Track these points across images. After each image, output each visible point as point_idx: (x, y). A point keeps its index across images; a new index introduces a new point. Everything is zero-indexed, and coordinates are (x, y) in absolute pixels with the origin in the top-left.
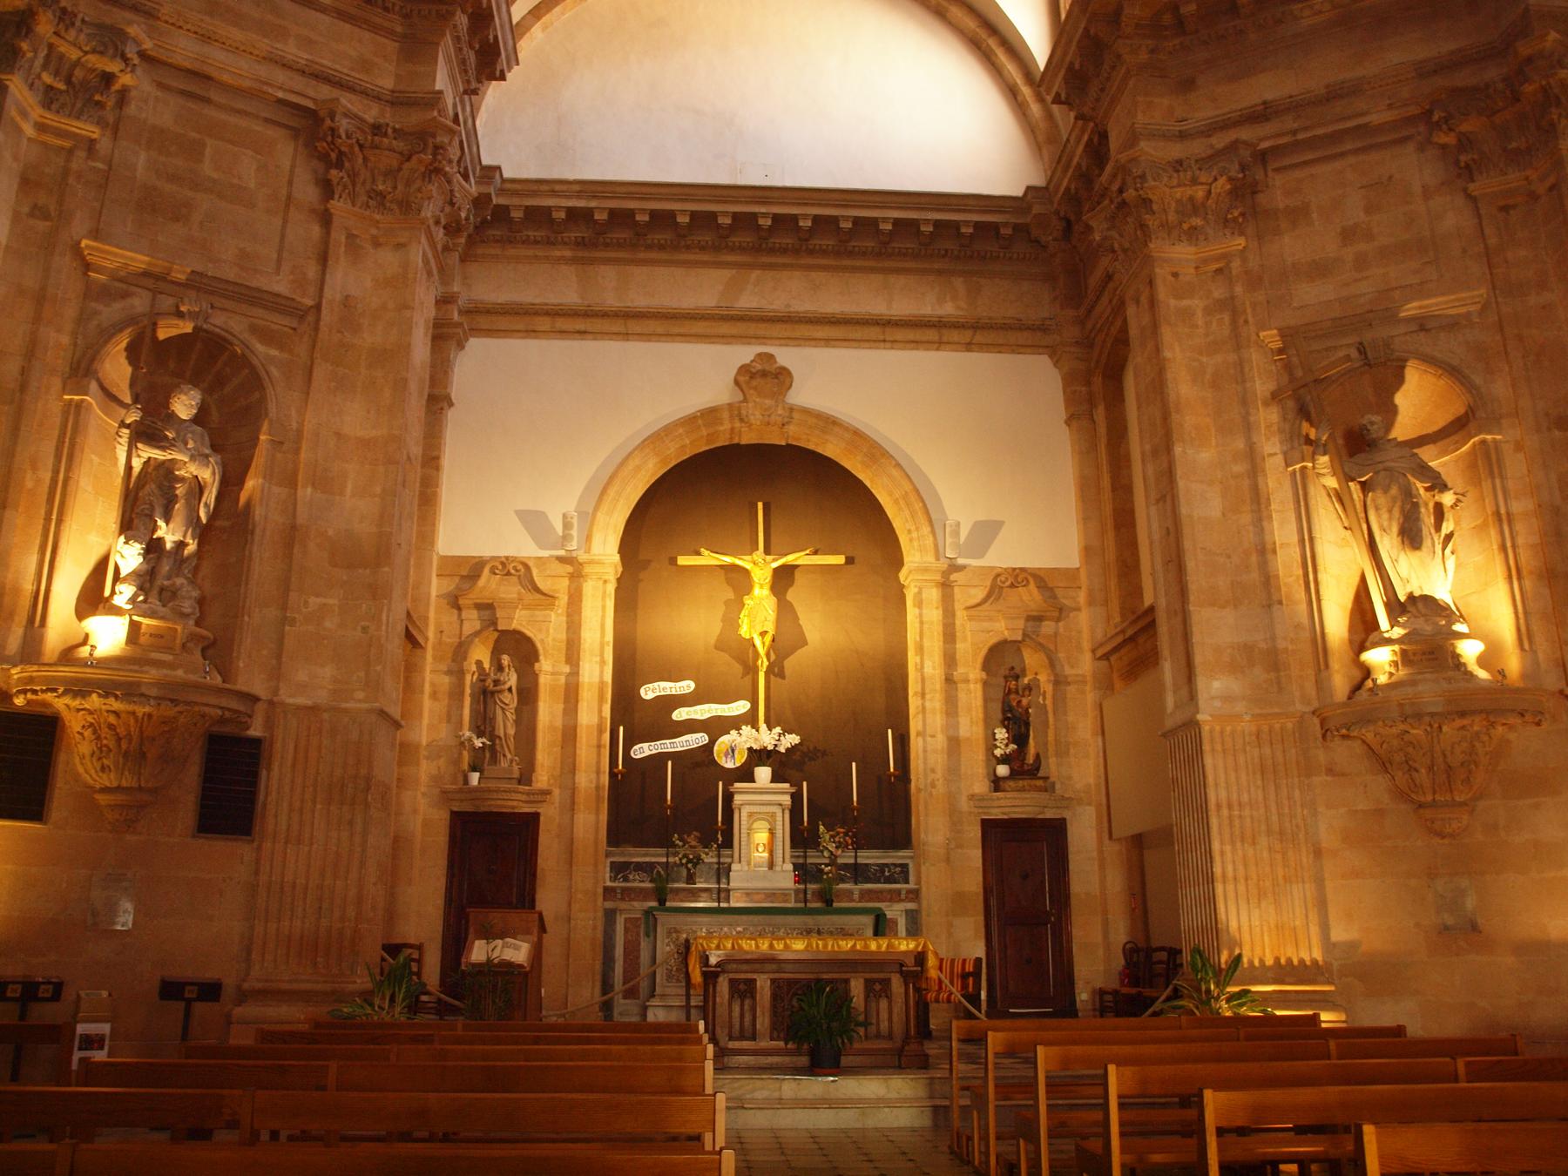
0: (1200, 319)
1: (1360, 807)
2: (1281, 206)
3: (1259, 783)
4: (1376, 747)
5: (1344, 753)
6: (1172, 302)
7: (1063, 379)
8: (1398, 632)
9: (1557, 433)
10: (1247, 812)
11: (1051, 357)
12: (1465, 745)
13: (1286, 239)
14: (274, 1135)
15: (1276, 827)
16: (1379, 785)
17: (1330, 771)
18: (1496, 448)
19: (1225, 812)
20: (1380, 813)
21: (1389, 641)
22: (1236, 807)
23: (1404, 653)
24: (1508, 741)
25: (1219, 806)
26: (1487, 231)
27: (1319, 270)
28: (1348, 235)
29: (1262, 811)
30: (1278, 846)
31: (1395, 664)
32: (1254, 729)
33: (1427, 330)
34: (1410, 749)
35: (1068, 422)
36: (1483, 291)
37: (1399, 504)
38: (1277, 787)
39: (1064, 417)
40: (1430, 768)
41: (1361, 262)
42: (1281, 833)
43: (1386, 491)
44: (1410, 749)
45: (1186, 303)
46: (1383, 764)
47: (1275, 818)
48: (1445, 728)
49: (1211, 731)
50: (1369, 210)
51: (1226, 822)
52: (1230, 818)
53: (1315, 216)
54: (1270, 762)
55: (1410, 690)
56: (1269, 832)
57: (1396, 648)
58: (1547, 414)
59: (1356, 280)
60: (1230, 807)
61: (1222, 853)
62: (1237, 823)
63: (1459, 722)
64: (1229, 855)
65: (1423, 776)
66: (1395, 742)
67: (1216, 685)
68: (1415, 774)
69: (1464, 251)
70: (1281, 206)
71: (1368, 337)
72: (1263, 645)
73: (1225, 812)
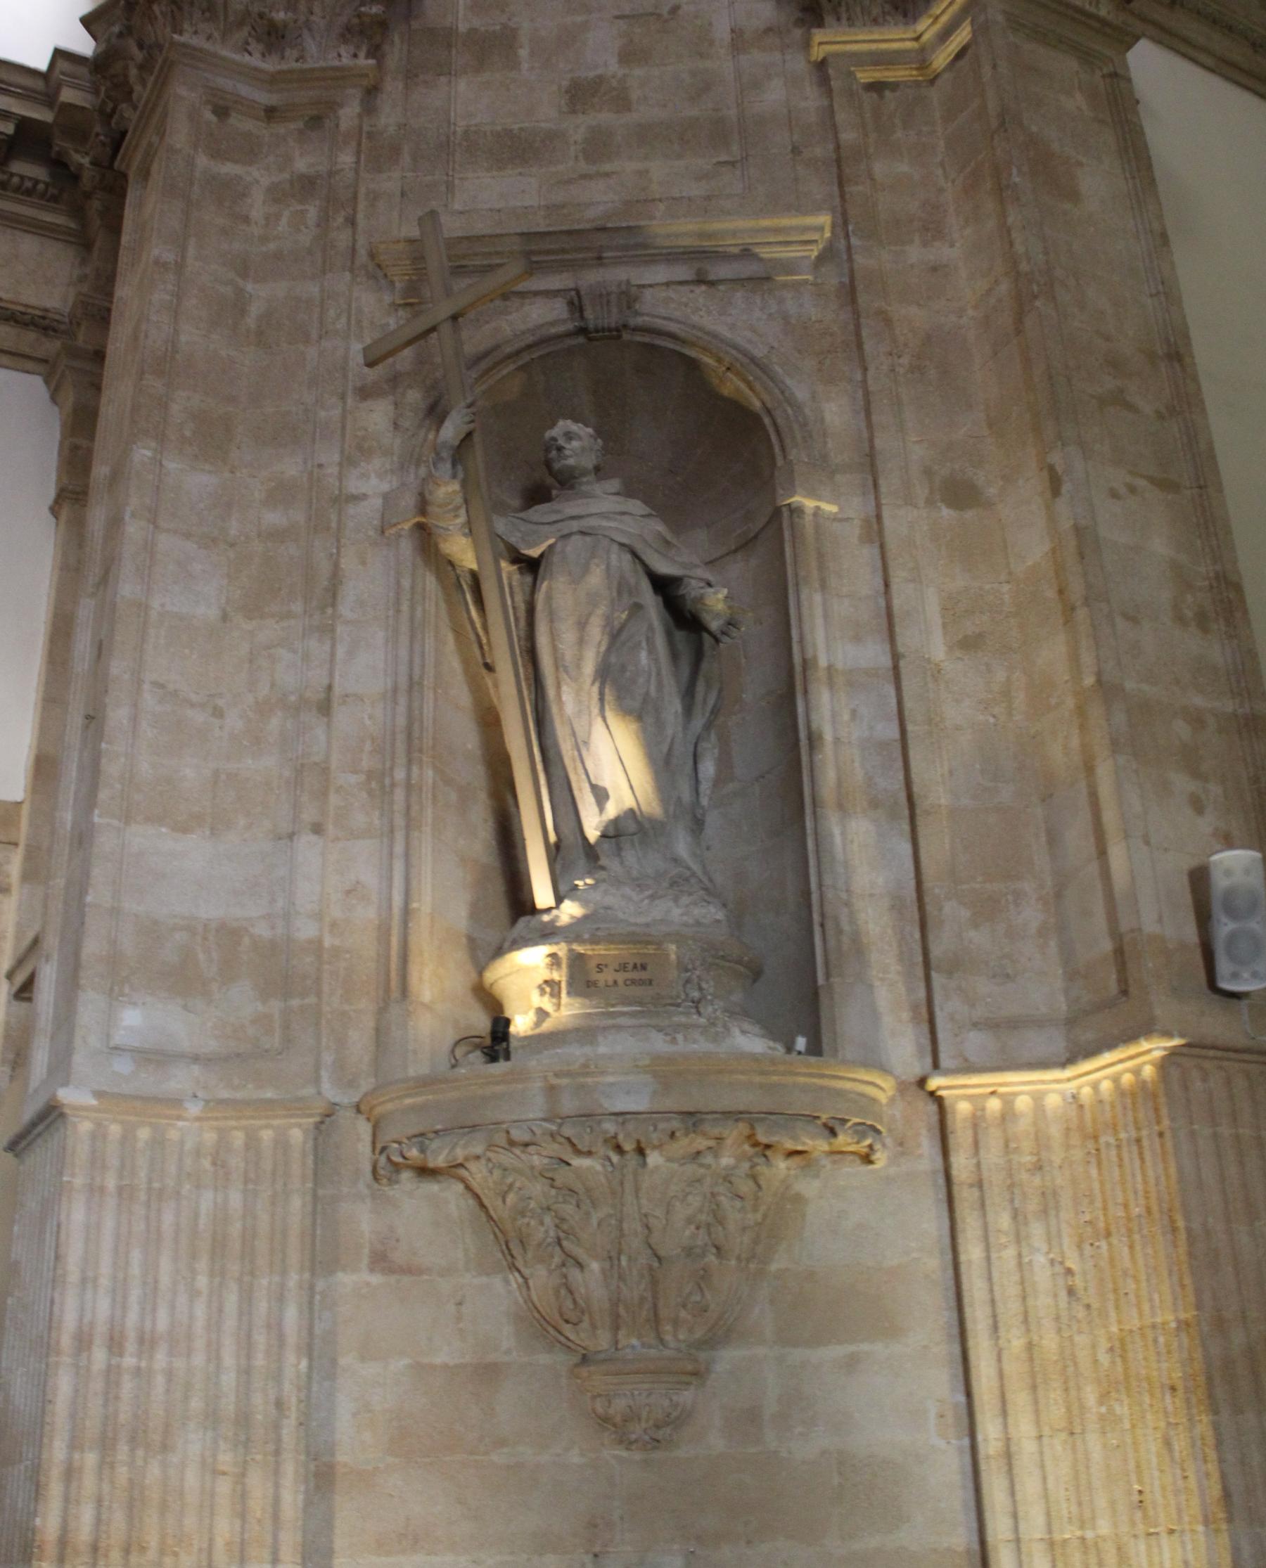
0: (257, 207)
1: (438, 1360)
2: (463, 27)
3: (202, 1281)
4: (499, 1209)
5: (423, 1217)
6: (202, 161)
7: (63, 425)
8: (570, 910)
9: (946, 512)
10: (161, 1358)
11: (47, 382)
12: (695, 1201)
13: (462, 85)
14: (1140, 1492)
15: (228, 1405)
16: (493, 1300)
17: (381, 1260)
18: (817, 527)
19: (99, 1356)
20: (487, 1373)
21: (548, 934)
22: (131, 1346)
23: (577, 961)
24: (798, 1199)
25: (83, 1342)
26: (841, 117)
27: (516, 149)
28: (581, 94)
29: (199, 1360)
30: (226, 1459)
31: (550, 987)
32: (210, 1137)
33: (712, 284)
34: (569, 1209)
35: (55, 511)
36: (824, 219)
37: (602, 610)
38: (247, 1297)
39: (51, 493)
40: (612, 1259)
41: (598, 147)
42: (243, 1419)
43: (576, 581)
44: (569, 1209)
45: (229, 169)
46: (505, 1244)
47: (229, 1380)
48: (654, 1158)
49: (98, 1135)
50: (628, 56)
51: (97, 1385)
52: (112, 1375)
53: (523, 53)
54: (235, 1229)
55: (577, 1053)
56: (212, 1418)
57: (561, 949)
58: (928, 472)
59: (584, 177)
60: (115, 1344)
61: (71, 1473)
62: (127, 1386)
63: (684, 1145)
64: (89, 1482)
65: (592, 1280)
66: (538, 1188)
67: (132, 1019)
68: (575, 1274)
69: (796, 150)
70: (463, 27)
71: (591, 278)
72: (262, 931)
73: (99, 1356)
